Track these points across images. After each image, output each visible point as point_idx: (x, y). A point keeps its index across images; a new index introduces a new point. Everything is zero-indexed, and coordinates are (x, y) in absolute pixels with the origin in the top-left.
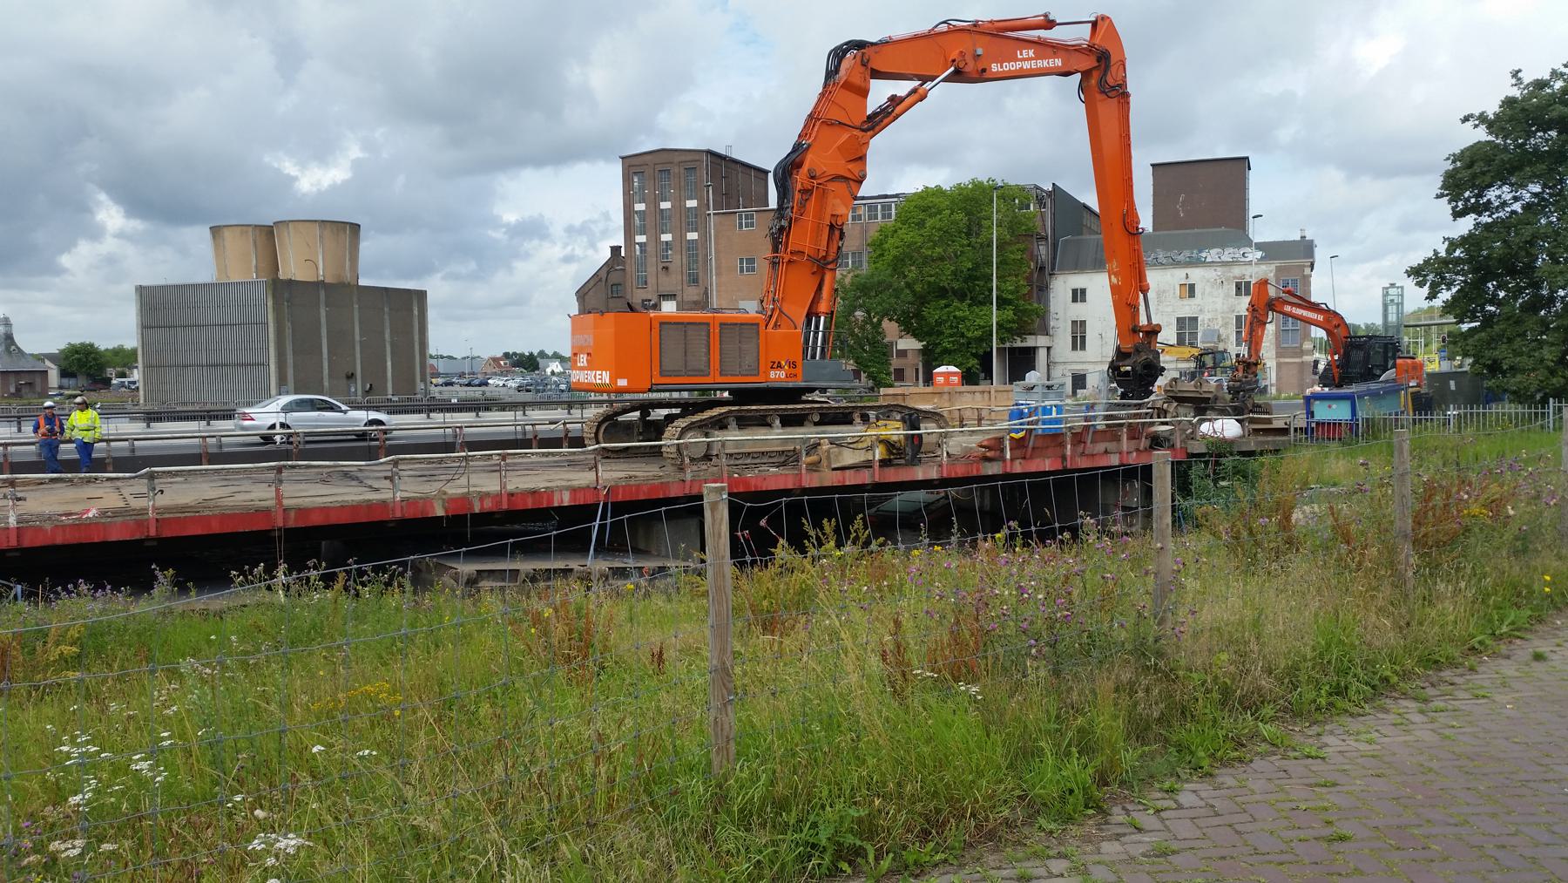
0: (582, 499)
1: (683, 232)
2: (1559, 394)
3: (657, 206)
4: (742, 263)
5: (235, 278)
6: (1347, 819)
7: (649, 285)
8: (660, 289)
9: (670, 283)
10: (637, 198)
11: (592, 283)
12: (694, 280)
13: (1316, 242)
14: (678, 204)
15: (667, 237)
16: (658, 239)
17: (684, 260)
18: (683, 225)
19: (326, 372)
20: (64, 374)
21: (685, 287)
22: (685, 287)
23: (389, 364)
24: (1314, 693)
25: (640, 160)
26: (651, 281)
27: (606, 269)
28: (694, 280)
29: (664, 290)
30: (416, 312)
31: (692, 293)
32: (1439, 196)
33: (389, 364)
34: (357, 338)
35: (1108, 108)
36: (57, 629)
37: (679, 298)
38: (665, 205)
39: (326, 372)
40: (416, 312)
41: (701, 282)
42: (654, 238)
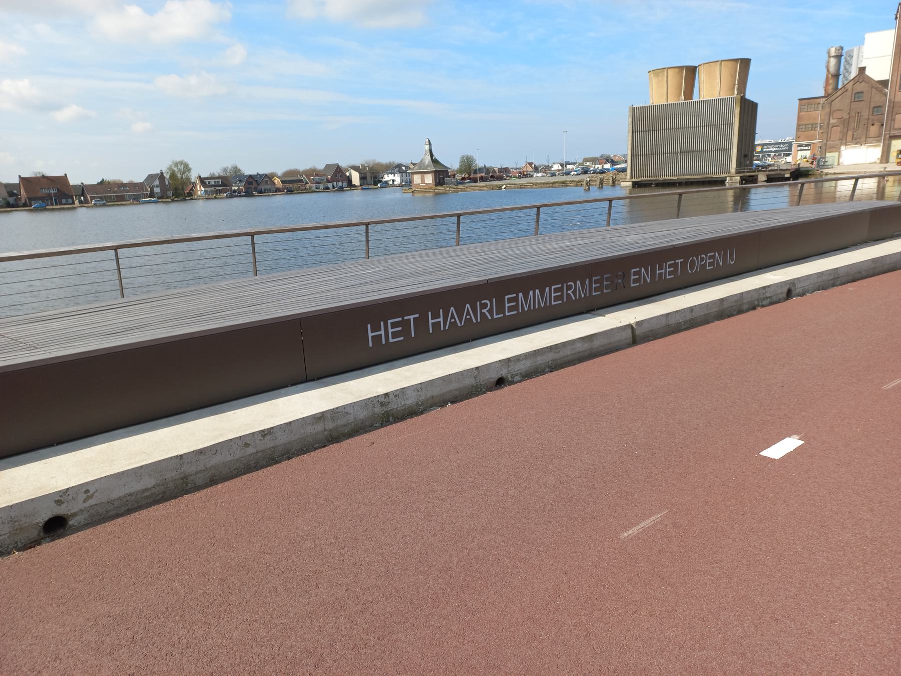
20: (363, 178)
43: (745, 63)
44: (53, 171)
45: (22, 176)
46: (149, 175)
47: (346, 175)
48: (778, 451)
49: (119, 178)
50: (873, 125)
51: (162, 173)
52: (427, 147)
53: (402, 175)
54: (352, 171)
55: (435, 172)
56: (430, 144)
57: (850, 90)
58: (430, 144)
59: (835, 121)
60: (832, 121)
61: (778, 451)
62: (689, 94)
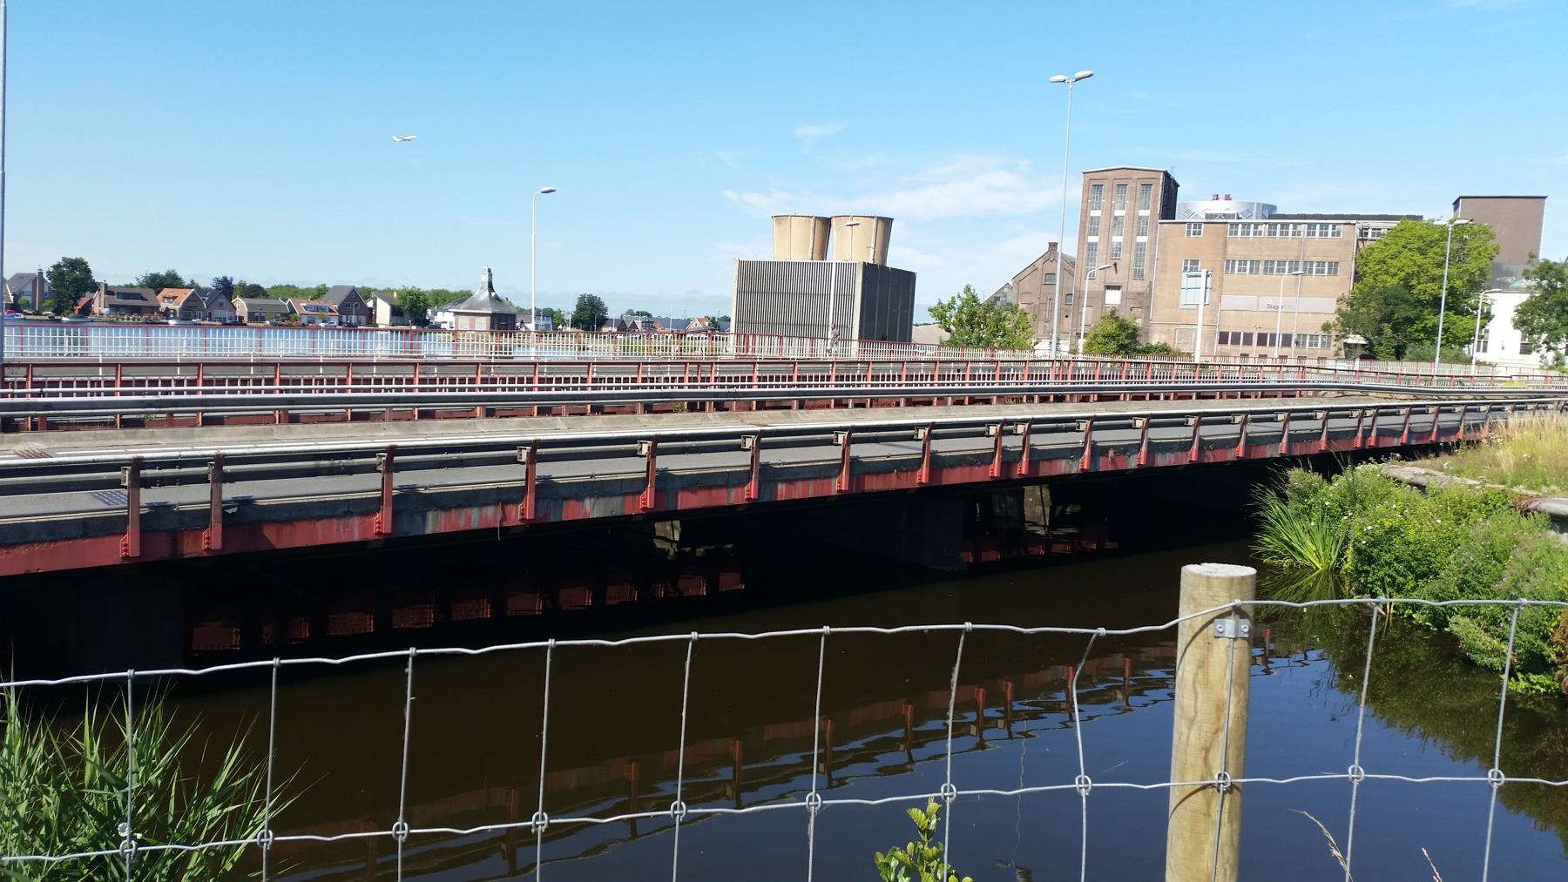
0: (1173, 461)
1: (1135, 234)
2: (1567, 410)
6: (1313, 650)
8: (1107, 280)
10: (1118, 205)
11: (1028, 271)
12: (1139, 275)
14: (1132, 212)
15: (1117, 239)
16: (1109, 239)
17: (1133, 259)
18: (1135, 229)
20: (396, 312)
21: (1131, 280)
22: (1131, 280)
27: (1042, 261)
28: (1139, 275)
29: (1110, 282)
31: (1137, 286)
32: (968, 289)
36: (200, 336)
37: (1123, 289)
41: (1145, 277)
42: (1106, 239)
43: (887, 223)
44: (257, 283)
45: (195, 282)
46: (17, 274)
47: (366, 306)
48: (730, 546)
49: (552, 307)
50: (1067, 317)
51: (41, 274)
52: (485, 278)
53: (378, 490)
54: (379, 301)
55: (493, 316)
56: (490, 275)
57: (1040, 267)
58: (490, 275)
61: (730, 546)
62: (823, 252)
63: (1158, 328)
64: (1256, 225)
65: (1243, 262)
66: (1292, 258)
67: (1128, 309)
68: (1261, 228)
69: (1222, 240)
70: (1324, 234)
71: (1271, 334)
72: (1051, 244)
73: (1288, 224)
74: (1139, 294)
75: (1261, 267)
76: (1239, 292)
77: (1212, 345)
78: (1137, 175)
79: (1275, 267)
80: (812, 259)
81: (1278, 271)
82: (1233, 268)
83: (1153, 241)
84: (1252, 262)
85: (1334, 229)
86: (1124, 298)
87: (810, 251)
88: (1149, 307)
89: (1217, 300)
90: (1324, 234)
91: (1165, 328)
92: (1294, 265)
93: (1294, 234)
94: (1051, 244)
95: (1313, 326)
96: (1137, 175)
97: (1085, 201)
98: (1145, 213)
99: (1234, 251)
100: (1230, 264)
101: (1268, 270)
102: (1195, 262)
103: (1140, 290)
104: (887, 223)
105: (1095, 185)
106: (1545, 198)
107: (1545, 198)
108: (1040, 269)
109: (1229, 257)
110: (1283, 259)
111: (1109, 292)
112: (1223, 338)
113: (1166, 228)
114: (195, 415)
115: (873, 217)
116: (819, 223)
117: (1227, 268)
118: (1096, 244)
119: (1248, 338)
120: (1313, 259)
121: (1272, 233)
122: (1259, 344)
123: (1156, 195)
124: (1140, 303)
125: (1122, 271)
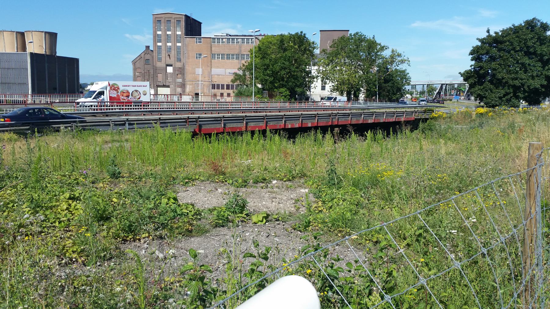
3: (165, 33)
4: (197, 55)
5: (48, 54)
7: (162, 61)
9: (172, 61)
11: (138, 58)
12: (179, 60)
13: (525, 20)
15: (169, 44)
17: (176, 53)
18: (176, 40)
19: (47, 87)
22: (176, 62)
23: (67, 85)
24: (412, 284)
25: (160, 16)
26: (163, 59)
27: (143, 54)
28: (179, 60)
29: (168, 63)
30: (76, 66)
31: (179, 65)
33: (67, 85)
34: (57, 75)
35: (326, 98)
37: (174, 66)
38: (169, 33)
39: (47, 87)
40: (76, 66)
41: (182, 61)
57: (143, 57)
59: (138, 74)
60: (137, 74)
63: (189, 83)
64: (222, 39)
65: (218, 55)
66: (236, 53)
67: (176, 75)
68: (224, 40)
69: (210, 45)
70: (233, 42)
71: (227, 85)
72: (146, 47)
73: (234, 38)
74: (180, 68)
75: (226, 57)
76: (218, 67)
77: (209, 89)
78: (174, 16)
79: (231, 57)
80: (17, 51)
81: (232, 58)
82: (215, 57)
83: (183, 45)
84: (222, 54)
85: (251, 40)
86: (174, 70)
87: (16, 48)
88: (184, 74)
89: (210, 71)
90: (233, 42)
91: (191, 83)
92: (238, 55)
93: (237, 43)
94: (146, 47)
95: (227, 80)
96: (174, 16)
97: (154, 27)
98: (179, 33)
99: (215, 50)
100: (213, 56)
101: (228, 58)
102: (200, 55)
103: (180, 66)
104: (22, 34)
105: (158, 20)
106: (349, 31)
107: (349, 31)
108: (143, 57)
109: (213, 53)
110: (229, 53)
111: (168, 68)
112: (214, 87)
113: (191, 41)
114: (124, 122)
115: (43, 32)
116: (19, 36)
117: (213, 57)
118: (161, 46)
119: (223, 86)
120: (225, 53)
121: (228, 42)
122: (227, 89)
123: (183, 25)
124: (181, 72)
125: (173, 59)
